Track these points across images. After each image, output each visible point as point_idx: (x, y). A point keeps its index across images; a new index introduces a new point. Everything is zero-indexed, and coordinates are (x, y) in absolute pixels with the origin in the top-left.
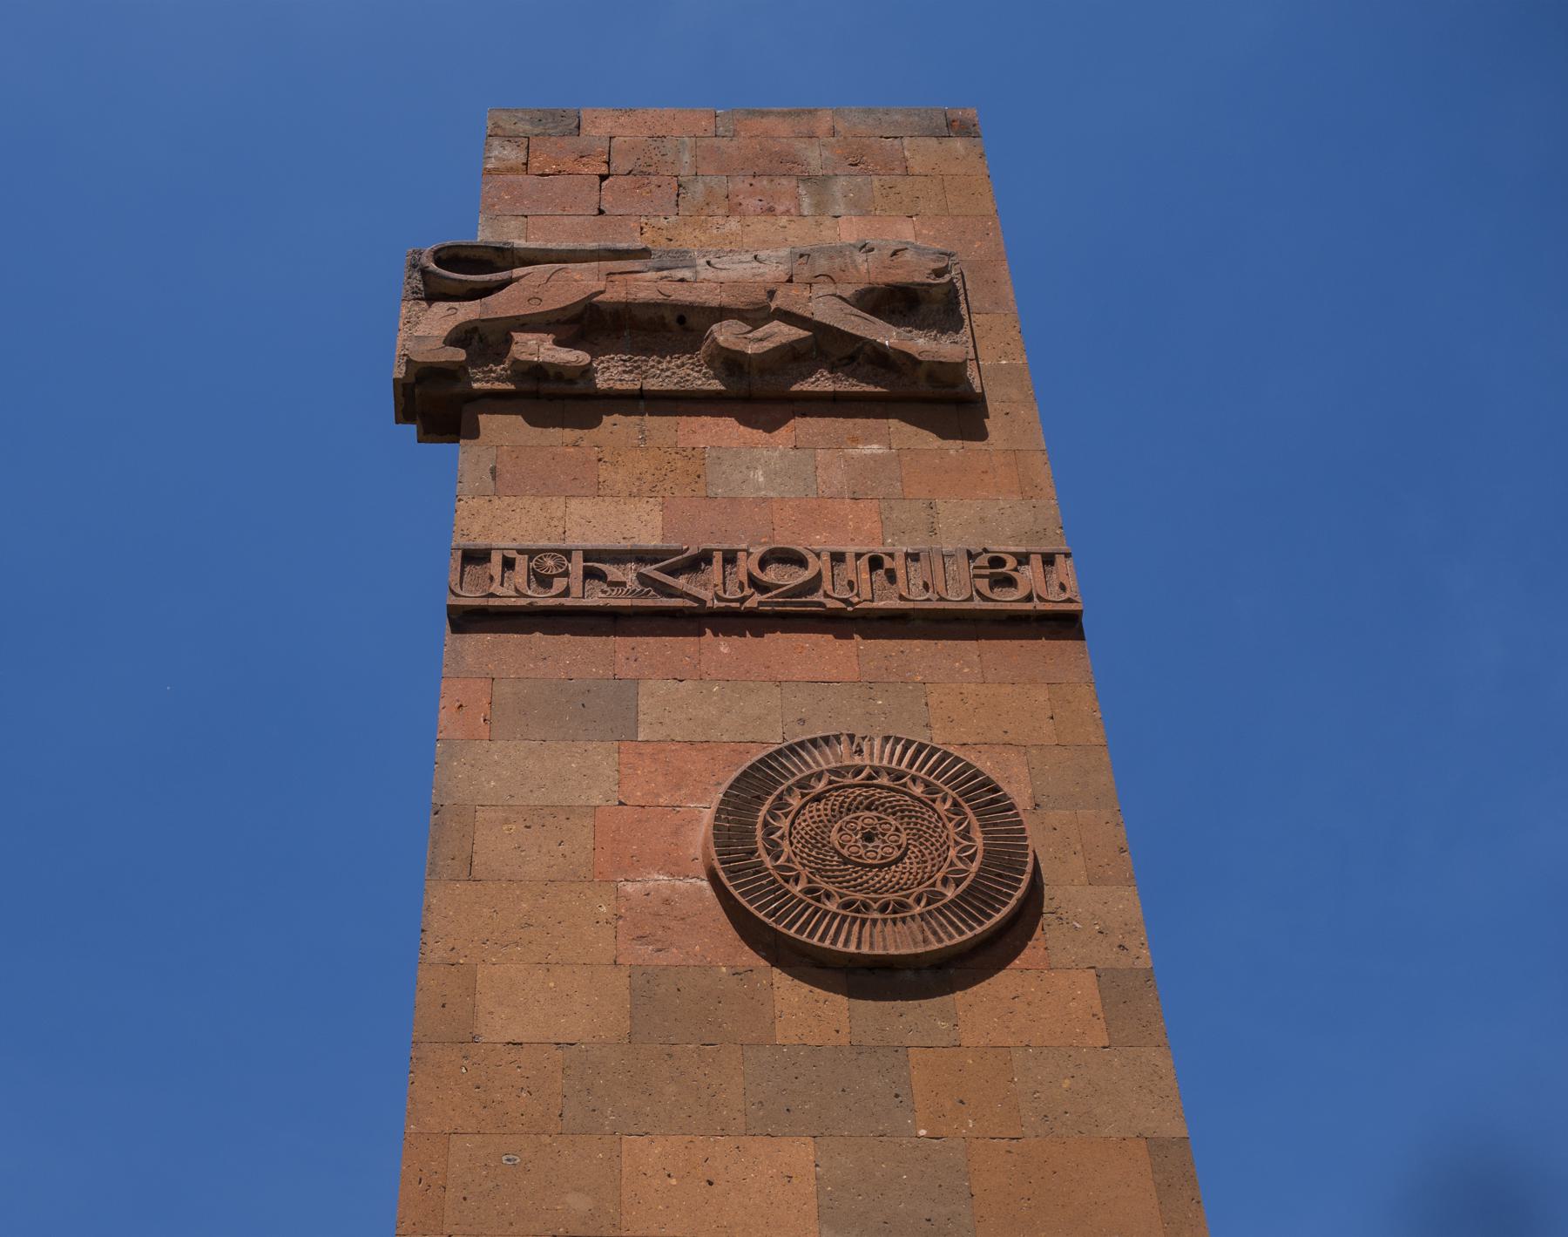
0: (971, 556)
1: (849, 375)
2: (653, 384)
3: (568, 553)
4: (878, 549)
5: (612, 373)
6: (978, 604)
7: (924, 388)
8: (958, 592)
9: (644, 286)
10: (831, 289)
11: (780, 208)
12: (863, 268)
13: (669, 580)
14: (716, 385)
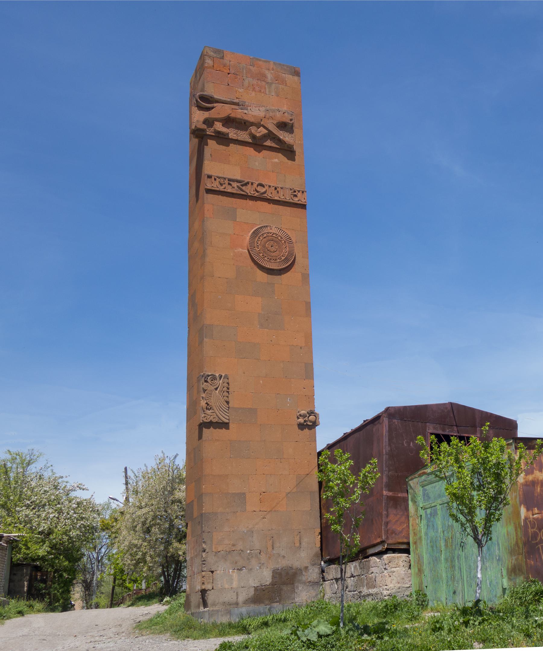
0: (291, 189)
1: (274, 142)
2: (240, 138)
3: (225, 179)
4: (277, 186)
5: (232, 133)
6: (291, 201)
7: (286, 148)
8: (288, 198)
9: (238, 113)
10: (272, 121)
11: (262, 91)
12: (278, 116)
13: (241, 187)
14: (250, 140)
